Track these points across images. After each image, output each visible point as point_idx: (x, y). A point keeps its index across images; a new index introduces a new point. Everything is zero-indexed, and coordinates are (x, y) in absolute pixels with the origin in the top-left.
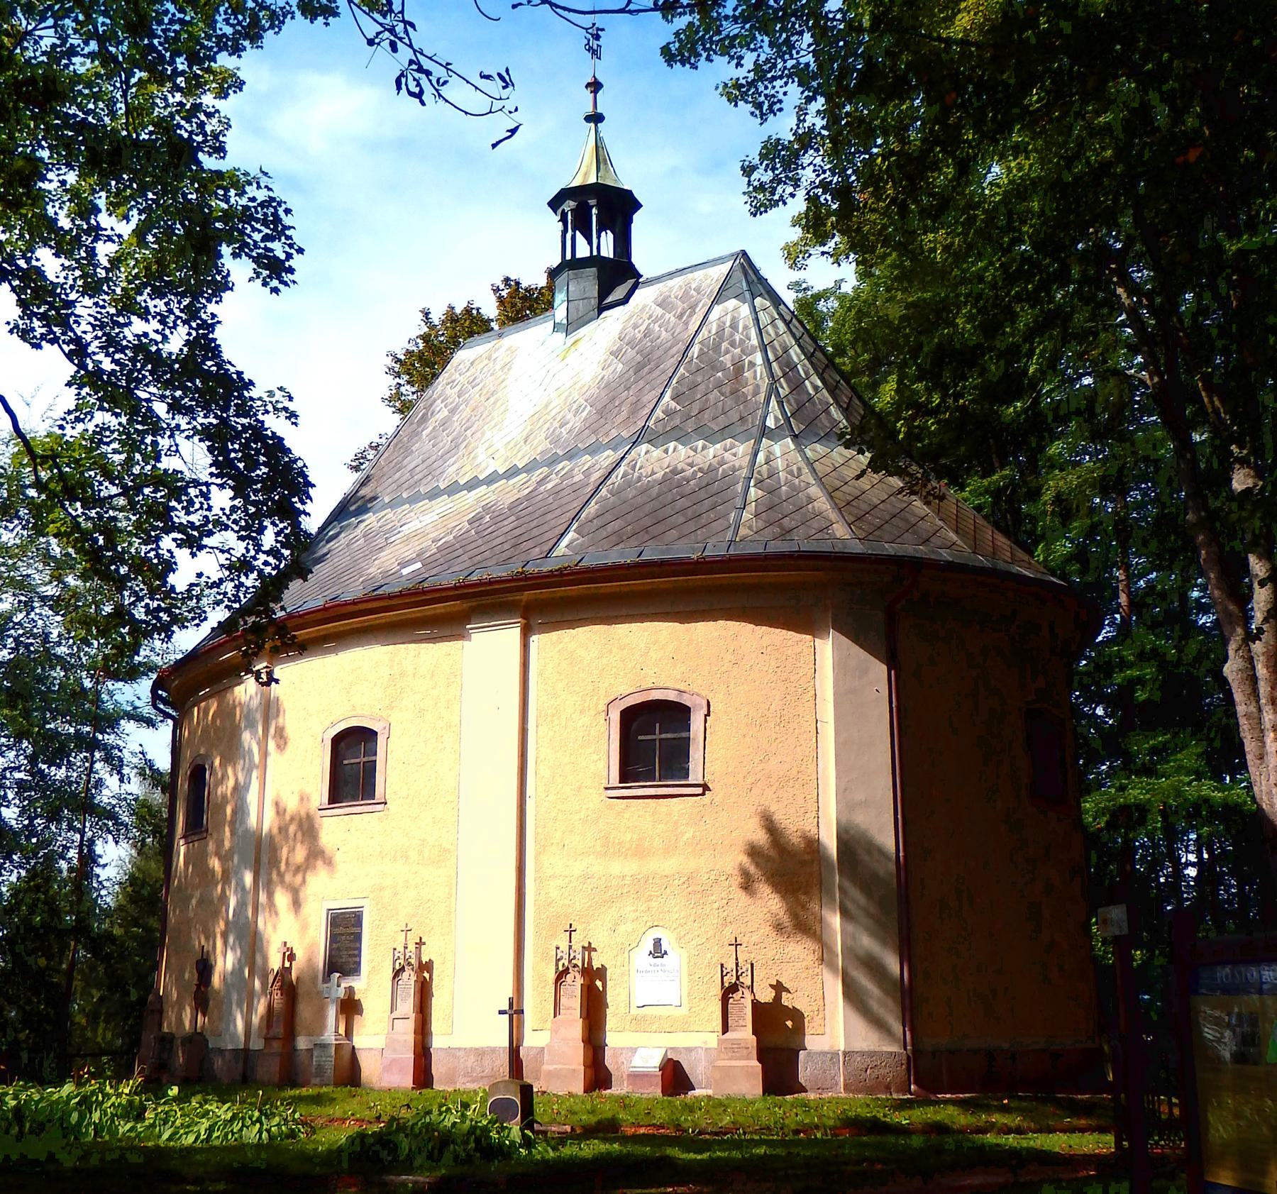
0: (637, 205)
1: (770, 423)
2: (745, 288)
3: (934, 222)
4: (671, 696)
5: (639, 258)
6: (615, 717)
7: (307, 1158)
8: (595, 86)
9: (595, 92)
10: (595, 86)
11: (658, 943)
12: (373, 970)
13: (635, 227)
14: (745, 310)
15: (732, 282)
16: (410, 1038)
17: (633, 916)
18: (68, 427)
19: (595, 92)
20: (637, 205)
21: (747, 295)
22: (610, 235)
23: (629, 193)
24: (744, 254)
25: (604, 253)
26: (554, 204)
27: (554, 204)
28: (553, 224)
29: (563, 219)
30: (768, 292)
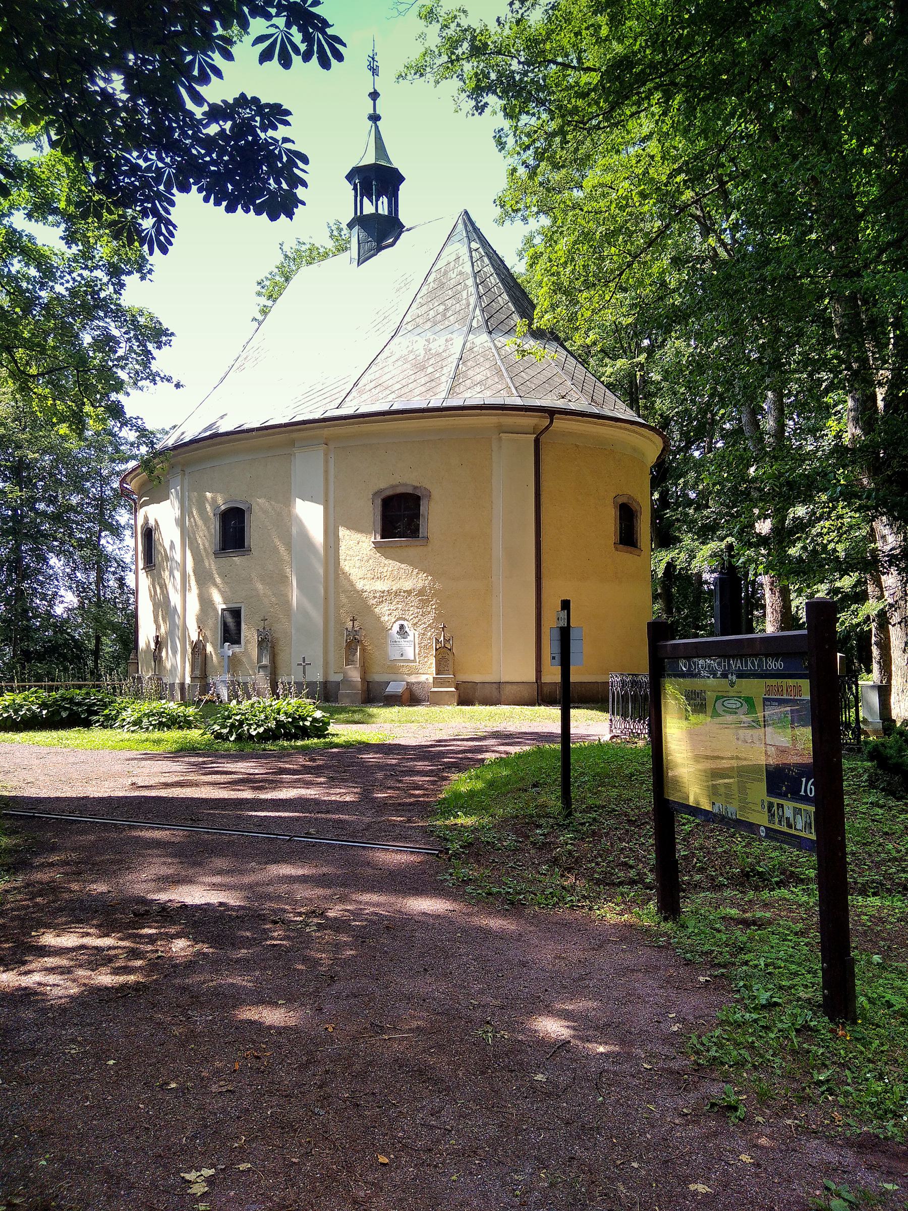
0: (401, 179)
1: (475, 324)
2: (465, 235)
3: (793, 128)
4: (410, 491)
5: (404, 216)
6: (379, 502)
7: (652, 741)
8: (374, 95)
9: (374, 100)
10: (374, 95)
11: (402, 627)
12: (247, 642)
13: (401, 193)
14: (465, 250)
15: (457, 230)
16: (572, 668)
17: (388, 612)
18: (641, 152)
19: (374, 100)
20: (401, 179)
21: (466, 240)
22: (385, 200)
23: (396, 171)
24: (466, 212)
25: (380, 211)
26: (349, 177)
27: (349, 177)
28: (347, 191)
29: (355, 189)
30: (479, 238)
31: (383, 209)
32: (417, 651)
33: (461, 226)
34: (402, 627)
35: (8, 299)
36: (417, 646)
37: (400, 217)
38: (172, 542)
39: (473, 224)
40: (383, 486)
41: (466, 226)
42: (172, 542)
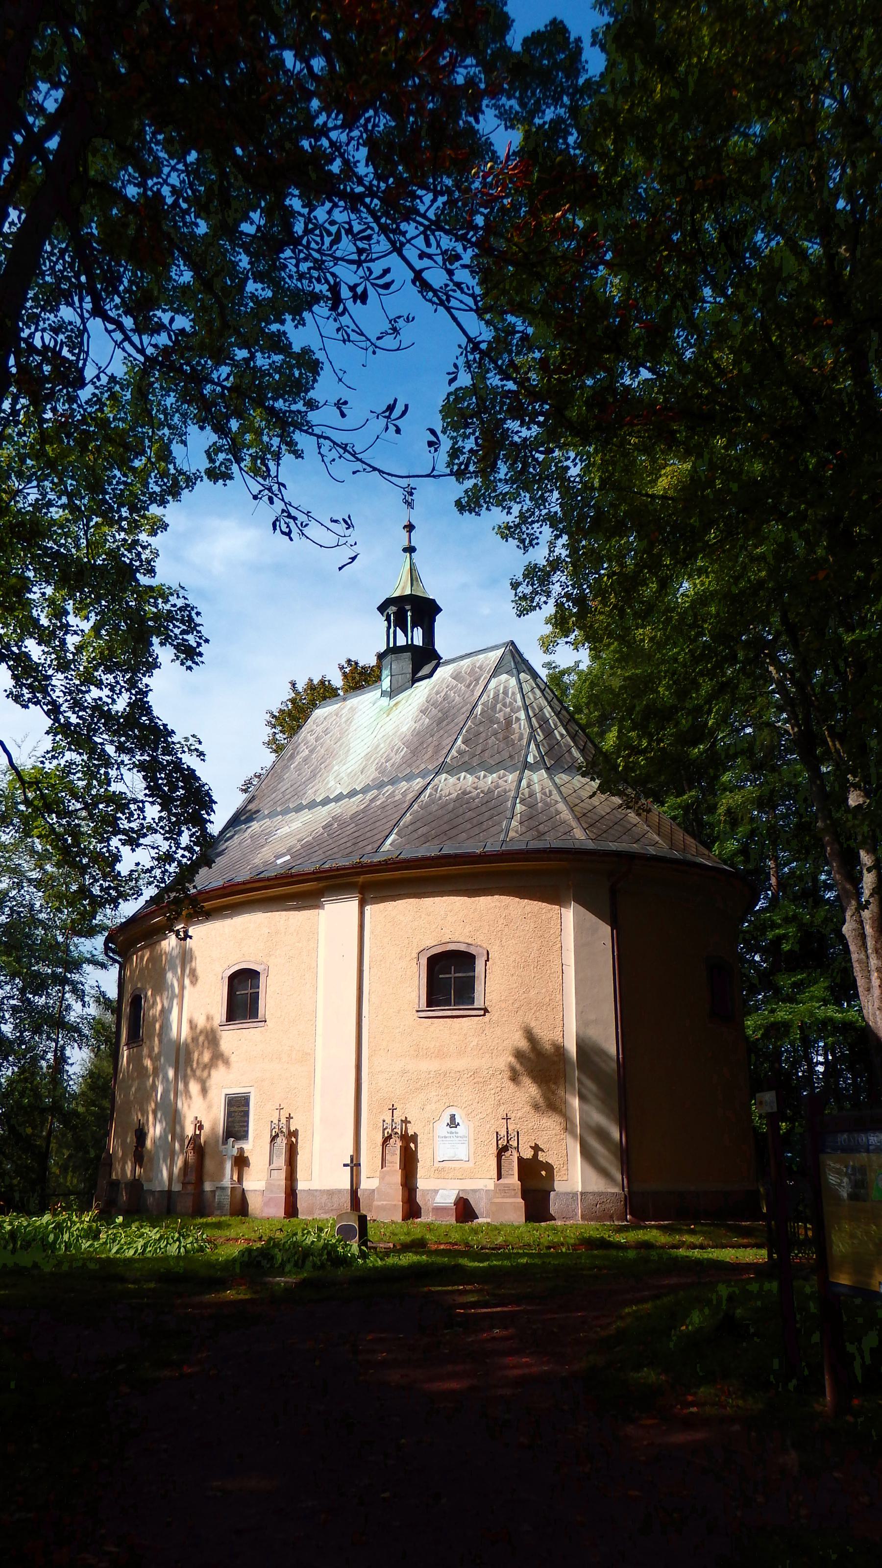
0: (438, 610)
4: (463, 948)
5: (440, 646)
6: (424, 962)
8: (410, 528)
9: (410, 532)
10: (410, 528)
11: (453, 1117)
14: (513, 682)
17: (436, 1099)
19: (410, 532)
20: (438, 610)
21: (515, 671)
24: (512, 643)
25: (416, 643)
26: (382, 609)
27: (382, 609)
29: (388, 619)
31: (418, 640)
32: (472, 1151)
33: (509, 657)
34: (453, 1117)
35: (144, 785)
36: (472, 1143)
37: (436, 647)
38: (393, 281)
39: (521, 655)
40: (430, 943)
41: (514, 657)
42: (393, 281)
